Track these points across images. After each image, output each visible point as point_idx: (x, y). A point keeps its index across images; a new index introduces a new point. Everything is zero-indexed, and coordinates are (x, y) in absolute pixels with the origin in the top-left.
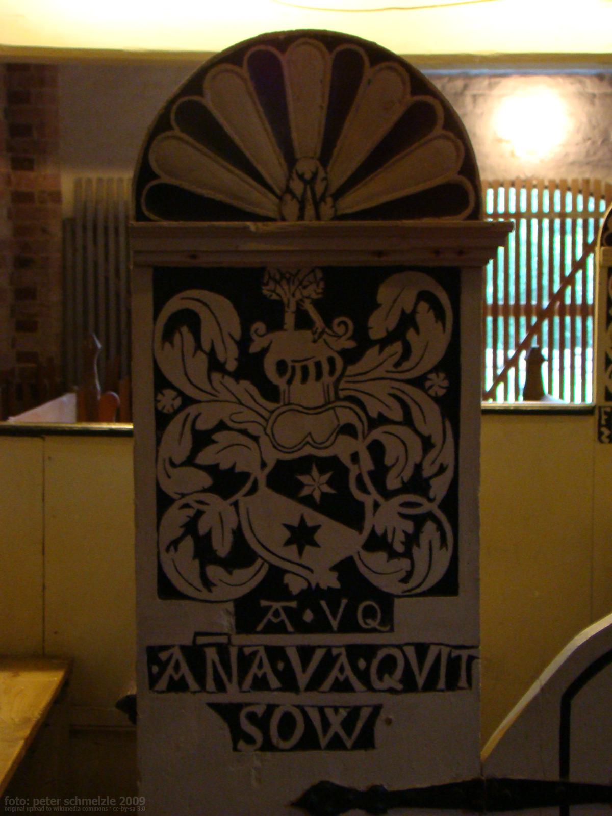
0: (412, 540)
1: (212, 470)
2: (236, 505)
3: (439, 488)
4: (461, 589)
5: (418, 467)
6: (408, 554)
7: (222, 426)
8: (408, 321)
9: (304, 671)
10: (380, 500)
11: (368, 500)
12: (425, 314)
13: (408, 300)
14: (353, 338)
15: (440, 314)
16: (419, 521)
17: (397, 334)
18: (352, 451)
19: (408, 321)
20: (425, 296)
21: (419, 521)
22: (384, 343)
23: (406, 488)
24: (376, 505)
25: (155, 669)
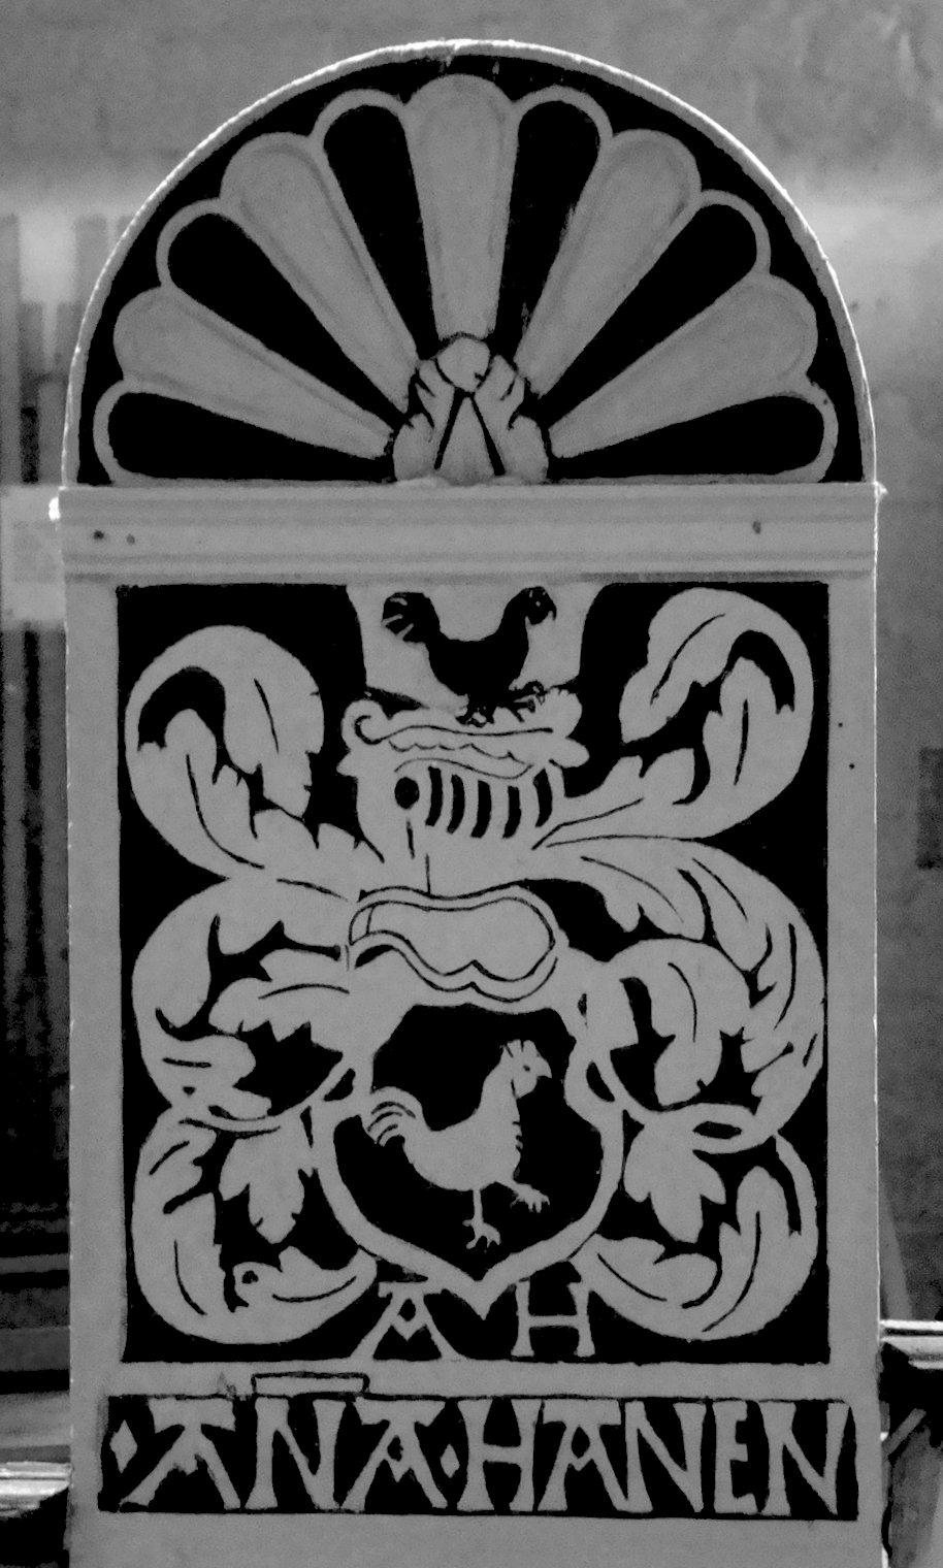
0: (718, 1215)
1: (258, 1038)
2: (306, 1118)
3: (781, 1095)
4: (488, 1447)
5: (732, 1045)
6: (708, 1245)
7: (277, 939)
8: (704, 699)
9: (821, 1472)
10: (638, 1112)
11: (604, 1118)
12: (748, 683)
13: (702, 665)
14: (577, 735)
15: (784, 693)
16: (731, 1169)
17: (684, 730)
18: (532, 1070)
19: (704, 699)
20: (753, 646)
21: (731, 1169)
22: (650, 750)
23: (708, 1094)
24: (632, 1128)
25: (125, 1445)
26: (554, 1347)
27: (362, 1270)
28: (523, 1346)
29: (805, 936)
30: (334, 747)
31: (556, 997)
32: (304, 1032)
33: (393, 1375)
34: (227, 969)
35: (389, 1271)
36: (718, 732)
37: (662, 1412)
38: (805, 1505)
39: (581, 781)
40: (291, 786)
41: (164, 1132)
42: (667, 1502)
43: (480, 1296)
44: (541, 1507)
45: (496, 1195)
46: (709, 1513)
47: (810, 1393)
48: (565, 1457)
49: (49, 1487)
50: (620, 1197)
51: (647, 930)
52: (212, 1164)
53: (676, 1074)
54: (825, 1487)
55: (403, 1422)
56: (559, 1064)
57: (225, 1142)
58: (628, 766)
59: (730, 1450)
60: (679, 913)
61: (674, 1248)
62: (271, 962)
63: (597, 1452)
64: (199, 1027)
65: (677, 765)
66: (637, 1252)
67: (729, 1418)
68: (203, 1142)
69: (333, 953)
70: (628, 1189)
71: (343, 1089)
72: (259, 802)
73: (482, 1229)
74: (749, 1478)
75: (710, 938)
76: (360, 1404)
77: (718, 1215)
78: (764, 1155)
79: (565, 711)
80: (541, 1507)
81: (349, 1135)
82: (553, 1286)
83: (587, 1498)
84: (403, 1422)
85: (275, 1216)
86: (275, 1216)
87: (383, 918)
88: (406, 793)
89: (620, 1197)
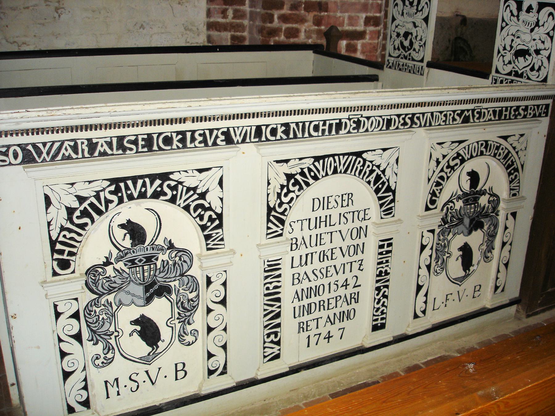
3: (424, 40)
8: (423, 7)
17: (422, 10)
19: (423, 7)
22: (420, 11)
26: (409, 59)
27: (400, 51)
28: (408, 59)
29: (426, 29)
30: (403, 10)
31: (412, 31)
32: (399, 33)
33: (401, 60)
34: (396, 27)
35: (402, 52)
36: (424, 10)
37: (414, 65)
38: (421, 74)
39: (416, 13)
40: (401, 13)
41: (392, 38)
42: (414, 73)
43: (406, 54)
44: (250, 127)
45: (408, 47)
46: (416, 74)
47: (422, 65)
48: (409, 68)
49: (502, 219)
50: (414, 48)
51: (418, 26)
52: (394, 42)
53: (419, 38)
54: (422, 73)
55: (401, 64)
56: (412, 36)
57: (395, 40)
58: (419, 12)
59: (418, 69)
60: (420, 26)
61: (416, 52)
62: (399, 26)
63: (411, 68)
64: (394, 31)
65: (421, 12)
66: (414, 52)
67: (418, 66)
68: (393, 40)
69: (401, 26)
70: (210, 326)
71: (401, 37)
72: (399, 14)
73: (407, 50)
74: (418, 71)
75: (421, 27)
76: (280, 333)
77: (419, 50)
78: (422, 46)
79: (415, 7)
80: (250, 127)
81: (401, 41)
82: (410, 54)
83: (410, 72)
84: (401, 64)
85: (396, 47)
86: (396, 47)
87: (405, 24)
88: (406, 14)
89: (414, 48)
